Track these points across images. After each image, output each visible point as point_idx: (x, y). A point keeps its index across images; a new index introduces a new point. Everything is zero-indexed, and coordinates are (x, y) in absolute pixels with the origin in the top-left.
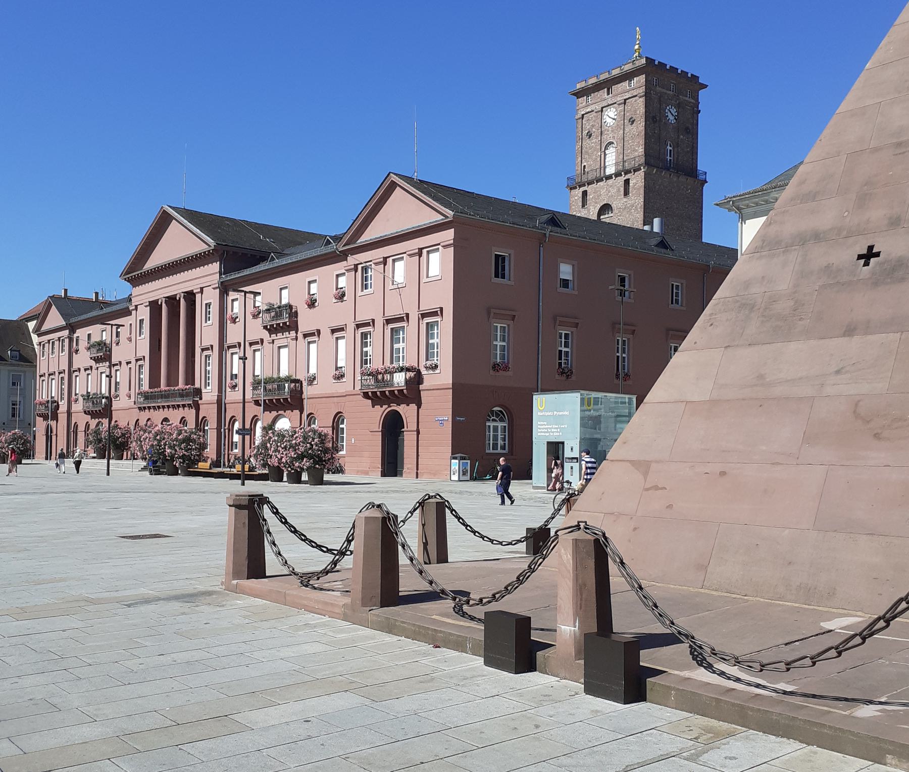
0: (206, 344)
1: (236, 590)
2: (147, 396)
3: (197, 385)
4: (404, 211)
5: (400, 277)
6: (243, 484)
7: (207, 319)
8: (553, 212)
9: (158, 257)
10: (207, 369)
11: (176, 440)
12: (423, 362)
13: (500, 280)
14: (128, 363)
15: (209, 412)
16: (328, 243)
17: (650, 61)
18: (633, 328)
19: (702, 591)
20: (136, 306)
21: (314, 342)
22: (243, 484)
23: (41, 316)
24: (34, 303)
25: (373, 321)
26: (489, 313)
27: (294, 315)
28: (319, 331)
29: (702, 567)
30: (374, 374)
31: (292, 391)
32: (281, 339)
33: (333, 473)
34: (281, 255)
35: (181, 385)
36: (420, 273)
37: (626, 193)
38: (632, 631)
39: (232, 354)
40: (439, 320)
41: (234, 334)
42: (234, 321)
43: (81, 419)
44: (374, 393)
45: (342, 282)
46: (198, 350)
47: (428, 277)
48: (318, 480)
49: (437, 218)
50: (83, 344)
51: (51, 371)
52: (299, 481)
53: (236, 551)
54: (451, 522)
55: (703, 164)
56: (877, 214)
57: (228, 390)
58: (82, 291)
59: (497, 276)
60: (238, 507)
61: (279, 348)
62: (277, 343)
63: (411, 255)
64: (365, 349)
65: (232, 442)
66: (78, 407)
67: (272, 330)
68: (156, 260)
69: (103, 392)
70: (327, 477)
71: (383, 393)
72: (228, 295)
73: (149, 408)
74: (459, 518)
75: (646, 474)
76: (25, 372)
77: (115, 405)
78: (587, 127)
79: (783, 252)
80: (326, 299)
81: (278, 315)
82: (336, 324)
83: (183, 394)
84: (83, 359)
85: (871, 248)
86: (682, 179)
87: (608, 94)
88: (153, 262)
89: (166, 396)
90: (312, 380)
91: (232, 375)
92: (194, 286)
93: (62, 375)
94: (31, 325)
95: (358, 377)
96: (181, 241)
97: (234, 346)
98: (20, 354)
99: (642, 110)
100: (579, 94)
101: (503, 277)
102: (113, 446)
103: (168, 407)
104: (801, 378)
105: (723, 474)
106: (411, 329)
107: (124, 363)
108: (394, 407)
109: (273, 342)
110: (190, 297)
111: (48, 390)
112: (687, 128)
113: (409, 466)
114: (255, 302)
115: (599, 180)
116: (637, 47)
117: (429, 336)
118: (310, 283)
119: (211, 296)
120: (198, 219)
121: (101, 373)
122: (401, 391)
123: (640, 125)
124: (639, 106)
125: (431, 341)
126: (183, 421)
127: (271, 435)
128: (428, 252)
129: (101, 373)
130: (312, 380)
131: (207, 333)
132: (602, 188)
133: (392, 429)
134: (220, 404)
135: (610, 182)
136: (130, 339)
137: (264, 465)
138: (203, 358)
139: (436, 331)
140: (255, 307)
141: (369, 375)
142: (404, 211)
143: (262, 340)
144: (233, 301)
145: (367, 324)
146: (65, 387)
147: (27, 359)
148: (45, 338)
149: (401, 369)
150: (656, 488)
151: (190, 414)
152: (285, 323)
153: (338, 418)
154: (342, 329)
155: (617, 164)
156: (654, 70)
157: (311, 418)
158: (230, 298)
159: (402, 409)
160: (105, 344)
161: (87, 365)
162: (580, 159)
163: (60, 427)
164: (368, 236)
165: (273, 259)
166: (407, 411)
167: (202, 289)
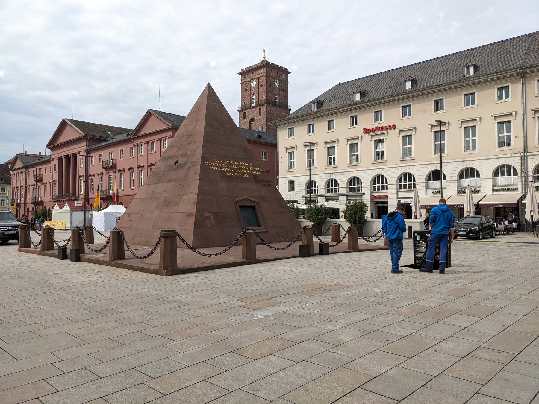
0: (80, 174)
8: (316, 99)
9: (63, 139)
37: (260, 114)
43: (31, 207)
46: (77, 177)
48: (354, 248)
51: (18, 186)
74: (183, 240)
82: (130, 167)
84: (31, 181)
92: (76, 151)
94: (10, 166)
99: (265, 82)
109: (107, 174)
115: (250, 108)
120: (77, 123)
123: (264, 88)
131: (81, 170)
135: (254, 109)
146: (23, 193)
148: (15, 172)
161: (100, 172)
164: (142, 133)
165: (108, 141)
167: (79, 152)
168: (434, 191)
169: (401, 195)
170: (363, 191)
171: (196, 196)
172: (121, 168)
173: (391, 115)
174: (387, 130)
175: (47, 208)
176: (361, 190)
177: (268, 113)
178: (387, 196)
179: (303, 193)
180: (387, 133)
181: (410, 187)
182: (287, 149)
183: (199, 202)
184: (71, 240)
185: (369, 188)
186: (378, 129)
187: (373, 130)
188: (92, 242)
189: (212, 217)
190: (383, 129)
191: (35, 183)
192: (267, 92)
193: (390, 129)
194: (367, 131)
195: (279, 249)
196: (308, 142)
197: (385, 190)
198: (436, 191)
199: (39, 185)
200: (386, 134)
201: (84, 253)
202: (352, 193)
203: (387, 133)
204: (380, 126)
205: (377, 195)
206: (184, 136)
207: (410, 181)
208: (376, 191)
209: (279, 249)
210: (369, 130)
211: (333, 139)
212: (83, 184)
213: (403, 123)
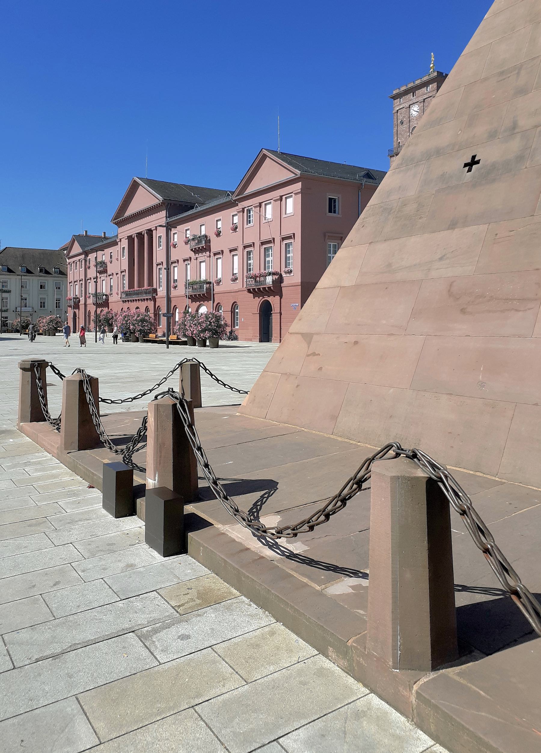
0: (159, 261)
2: (127, 294)
3: (155, 287)
4: (272, 172)
5: (269, 215)
6: (168, 348)
8: (368, 170)
9: (133, 209)
10: (159, 276)
12: (283, 269)
13: (332, 214)
14: (117, 274)
15: (162, 303)
16: (228, 195)
18: (341, 235)
19: (332, 436)
20: (121, 239)
21: (220, 258)
22: (168, 348)
25: (254, 243)
26: (325, 236)
27: (208, 241)
28: (222, 251)
29: (334, 418)
30: (255, 277)
32: (202, 256)
33: (232, 340)
34: (203, 204)
35: (146, 286)
36: (280, 211)
38: (235, 477)
39: (174, 267)
40: (293, 241)
41: (175, 255)
42: (175, 246)
43: (92, 308)
44: (254, 289)
46: (155, 265)
47: (286, 214)
49: (291, 176)
51: (75, 280)
52: (204, 345)
53: (22, 402)
54: (204, 377)
56: (481, 130)
57: (172, 289)
59: (330, 211)
60: (24, 369)
61: (200, 262)
62: (199, 260)
63: (275, 201)
64: (249, 262)
65: (175, 321)
68: (132, 210)
69: (104, 291)
71: (259, 289)
72: (171, 230)
73: (128, 301)
75: (309, 343)
76: (62, 281)
77: (111, 299)
79: (415, 166)
80: (227, 232)
81: (200, 242)
82: (232, 246)
83: (146, 292)
84: (92, 272)
85: (474, 157)
87: (413, 96)
88: (129, 212)
89: (138, 293)
90: (218, 282)
91: (174, 280)
92: (151, 226)
93: (81, 282)
95: (245, 279)
96: (145, 198)
97: (175, 262)
98: (60, 271)
100: (395, 97)
101: (335, 212)
102: (105, 324)
103: (139, 300)
104: (415, 265)
105: (356, 343)
106: (276, 247)
107: (115, 274)
108: (266, 298)
110: (150, 232)
111: (74, 291)
113: (276, 335)
114: (186, 235)
116: (432, 65)
117: (287, 252)
118: (217, 221)
119: (162, 232)
121: (103, 280)
122: (269, 288)
125: (288, 255)
126: (147, 310)
127: (188, 316)
128: (286, 198)
129: (103, 280)
130: (218, 282)
131: (159, 254)
133: (266, 312)
136: (117, 259)
137: (185, 336)
138: (158, 270)
139: (291, 249)
140: (186, 237)
141: (251, 278)
142: (272, 172)
143: (190, 258)
144: (174, 234)
145: (250, 246)
146: (83, 289)
147: (63, 274)
148: (72, 260)
149: (270, 274)
150: (314, 354)
151: (151, 304)
152: (203, 247)
153: (234, 306)
154: (236, 250)
157: (218, 307)
158: (173, 232)
159: (271, 299)
160: (104, 263)
161: (187, 257)
162: (396, 138)
163: (81, 313)
165: (197, 207)
166: (274, 300)
172: (219, 250)
175: (115, 311)
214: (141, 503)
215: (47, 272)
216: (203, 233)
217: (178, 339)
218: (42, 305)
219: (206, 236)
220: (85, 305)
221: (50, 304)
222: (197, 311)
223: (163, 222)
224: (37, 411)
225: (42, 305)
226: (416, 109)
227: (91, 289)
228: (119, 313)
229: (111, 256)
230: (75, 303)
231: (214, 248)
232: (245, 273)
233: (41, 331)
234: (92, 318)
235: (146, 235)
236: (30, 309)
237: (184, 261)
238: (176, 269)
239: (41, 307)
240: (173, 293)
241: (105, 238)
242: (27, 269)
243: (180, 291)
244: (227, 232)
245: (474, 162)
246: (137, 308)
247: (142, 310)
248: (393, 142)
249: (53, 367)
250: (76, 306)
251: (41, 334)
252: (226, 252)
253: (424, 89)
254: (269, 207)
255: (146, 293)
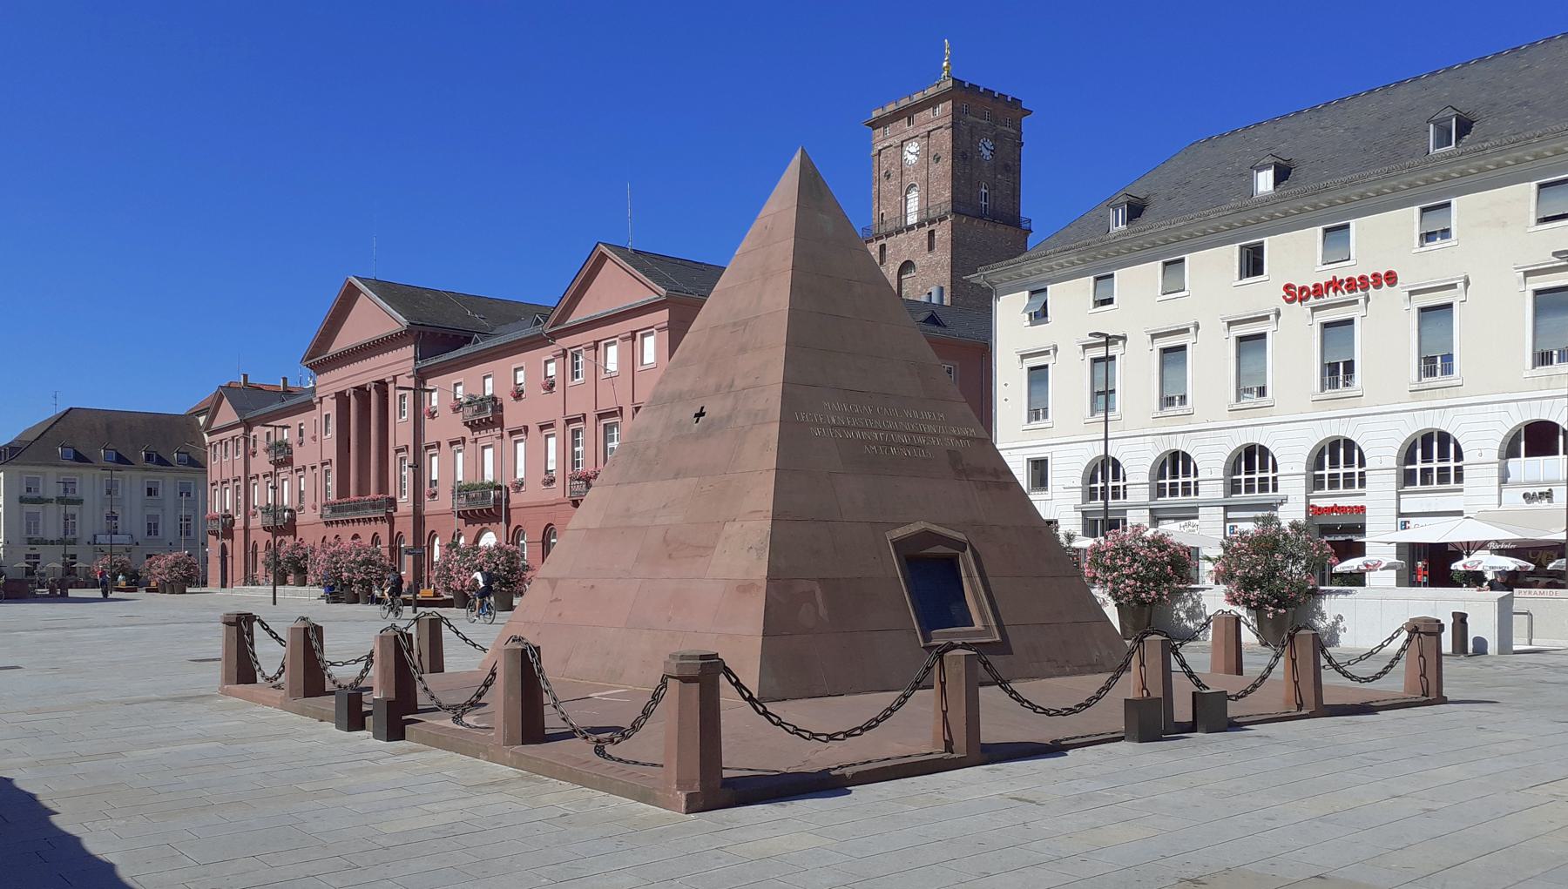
0: (400, 444)
1: (227, 693)
2: (335, 508)
3: (391, 494)
5: (612, 365)
7: (401, 414)
9: (346, 339)
11: (354, 561)
17: (958, 83)
23: (212, 410)
24: (205, 394)
27: (498, 408)
28: (526, 428)
31: (497, 500)
32: (486, 436)
34: (486, 335)
35: (373, 494)
36: (632, 359)
37: (931, 248)
41: (431, 433)
42: (432, 415)
43: (261, 538)
45: (552, 369)
46: (391, 452)
50: (261, 445)
51: (225, 478)
54: (446, 632)
55: (1027, 209)
58: (268, 377)
60: (228, 624)
62: (481, 443)
66: (256, 522)
67: (474, 426)
68: (342, 342)
70: (72, 593)
77: (300, 519)
78: (885, 165)
80: (534, 392)
81: (482, 409)
82: (544, 420)
83: (374, 505)
84: (261, 463)
86: (1001, 228)
89: (356, 508)
90: (519, 486)
94: (202, 419)
99: (949, 144)
110: (382, 386)
111: (222, 501)
112: (1007, 165)
123: (946, 165)
124: (945, 139)
126: (375, 539)
131: (401, 430)
132: (902, 240)
134: (418, 518)
135: (912, 233)
136: (314, 438)
137: (448, 589)
142: (617, 287)
146: (241, 497)
147: (197, 464)
154: (551, 426)
155: (920, 212)
156: (963, 93)
161: (457, 436)
163: (237, 547)
165: (477, 342)
168: (1531, 491)
169: (1410, 503)
170: (1280, 492)
171: (767, 525)
172: (519, 424)
173: (1385, 236)
174: (1365, 287)
175: (308, 542)
176: (1275, 489)
177: (957, 244)
178: (1362, 509)
179: (1077, 497)
180: (1367, 299)
181: (1443, 475)
182: (1023, 357)
183: (777, 546)
184: (376, 657)
185: (1302, 481)
186: (1335, 284)
187: (1318, 291)
188: (437, 665)
189: (818, 592)
190: (1351, 285)
191: (272, 468)
192: (955, 177)
193: (1378, 285)
194: (1294, 294)
195: (1058, 713)
196: (1101, 335)
197: (1357, 489)
198: (1537, 490)
199: (282, 476)
200: (1362, 301)
201: (417, 712)
202: (1242, 497)
203: (1367, 299)
204: (1342, 275)
205: (1328, 503)
206: (725, 326)
207: (1444, 456)
208: (1326, 491)
209: (1058, 713)
210: (1302, 289)
211: (1181, 325)
212: (408, 473)
213: (1423, 266)
214: (369, 720)
215: (162, 462)
216: (489, 392)
217: (436, 594)
218: (152, 529)
219: (494, 399)
220: (246, 530)
221: (168, 529)
222: (477, 541)
223: (410, 365)
224: (244, 669)
225: (152, 529)
226: (913, 150)
227: (257, 499)
228: (318, 546)
229: (301, 432)
230: (224, 526)
231: (511, 419)
232: (569, 472)
233: (153, 584)
234: (261, 556)
235: (373, 392)
236: (125, 539)
237: (452, 444)
238: (435, 459)
239: (149, 533)
240: (429, 506)
241: (288, 392)
242: (118, 455)
243: (441, 505)
244: (534, 392)
245: (701, 414)
246: (356, 536)
247: (366, 540)
248: (869, 211)
249: (262, 623)
250: (228, 532)
251: (156, 591)
252: (534, 429)
253: (929, 112)
254: (613, 350)
255: (373, 507)
